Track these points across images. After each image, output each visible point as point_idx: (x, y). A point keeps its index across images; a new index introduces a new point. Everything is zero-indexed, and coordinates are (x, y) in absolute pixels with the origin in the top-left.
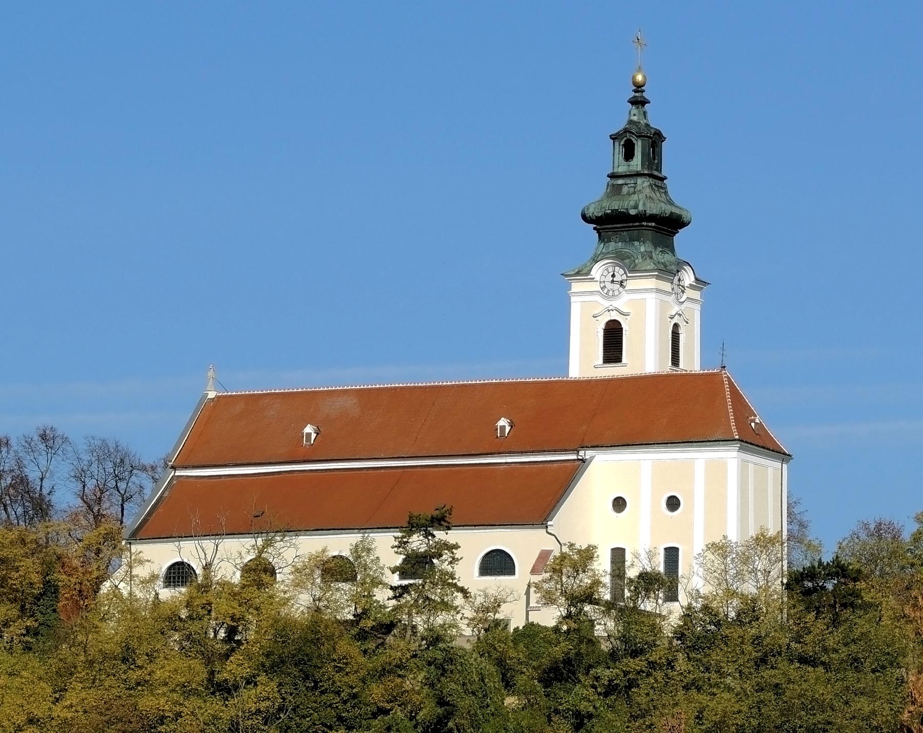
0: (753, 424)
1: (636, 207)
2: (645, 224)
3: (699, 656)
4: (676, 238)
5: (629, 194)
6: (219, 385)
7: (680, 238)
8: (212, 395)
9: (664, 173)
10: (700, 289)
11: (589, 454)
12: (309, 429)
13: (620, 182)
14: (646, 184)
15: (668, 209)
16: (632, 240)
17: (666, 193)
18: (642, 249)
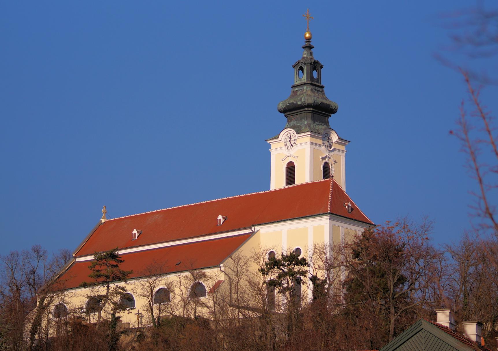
0: (347, 207)
1: (301, 100)
2: (306, 109)
3: (236, 322)
4: (330, 119)
5: (300, 95)
6: (107, 216)
7: (333, 119)
8: (103, 221)
9: (322, 84)
10: (344, 145)
11: (257, 228)
12: (135, 231)
13: (296, 89)
14: (309, 88)
15: (320, 100)
16: (301, 119)
17: (324, 94)
18: (306, 123)
